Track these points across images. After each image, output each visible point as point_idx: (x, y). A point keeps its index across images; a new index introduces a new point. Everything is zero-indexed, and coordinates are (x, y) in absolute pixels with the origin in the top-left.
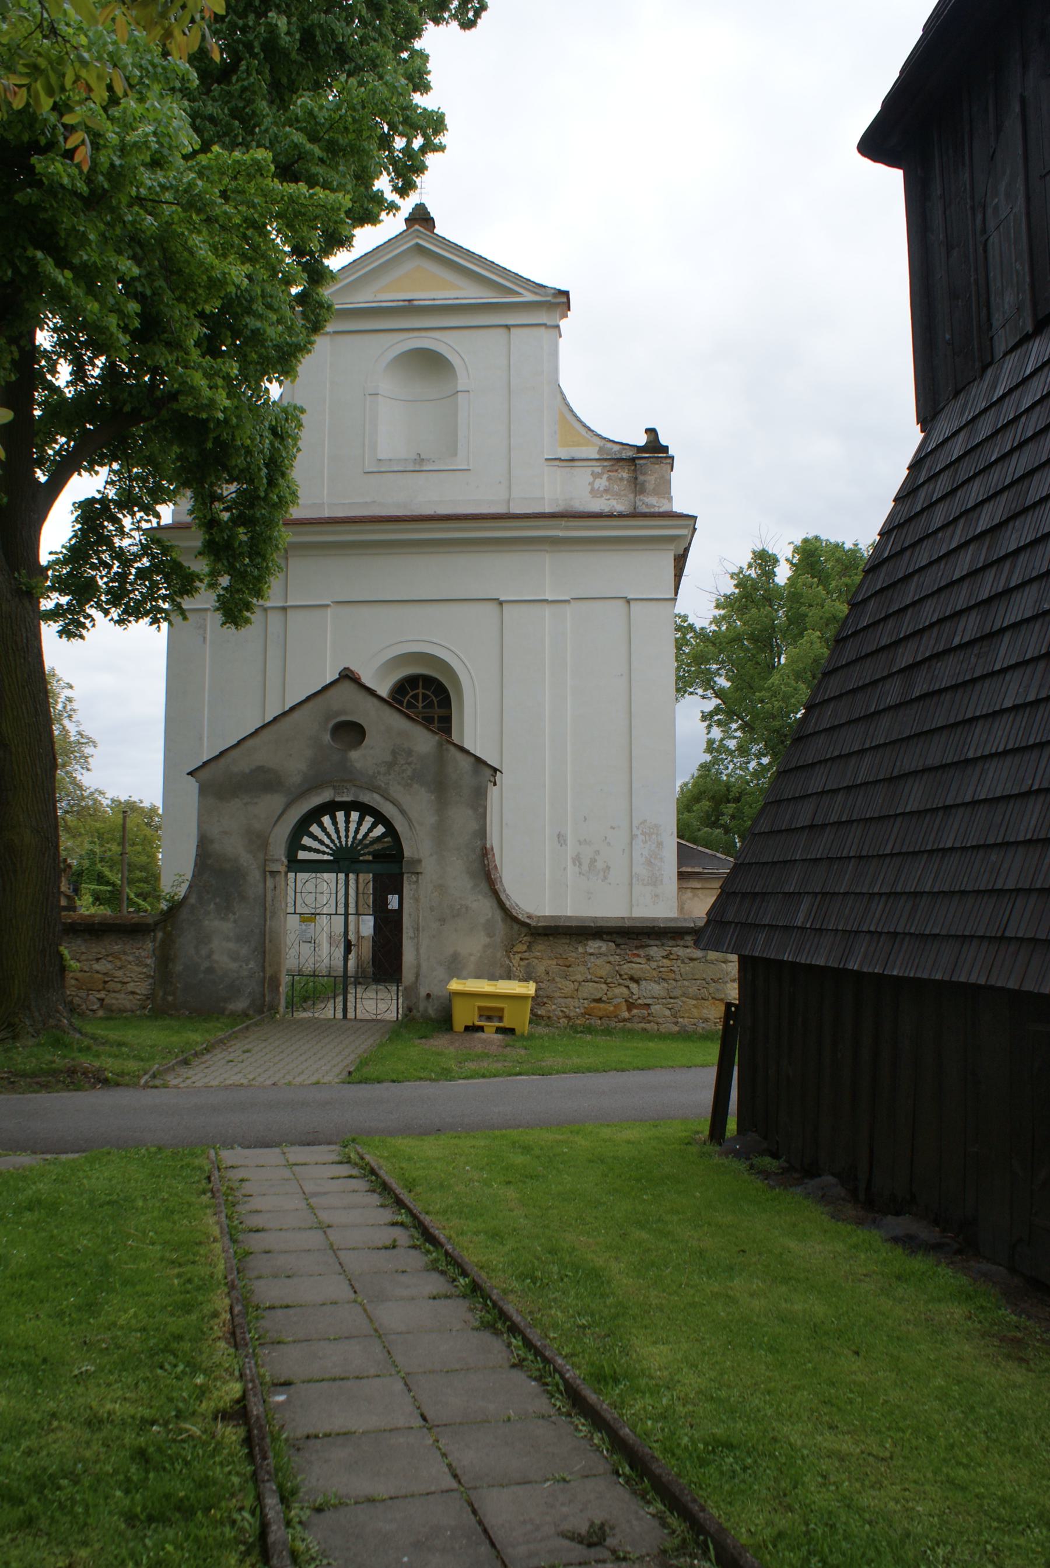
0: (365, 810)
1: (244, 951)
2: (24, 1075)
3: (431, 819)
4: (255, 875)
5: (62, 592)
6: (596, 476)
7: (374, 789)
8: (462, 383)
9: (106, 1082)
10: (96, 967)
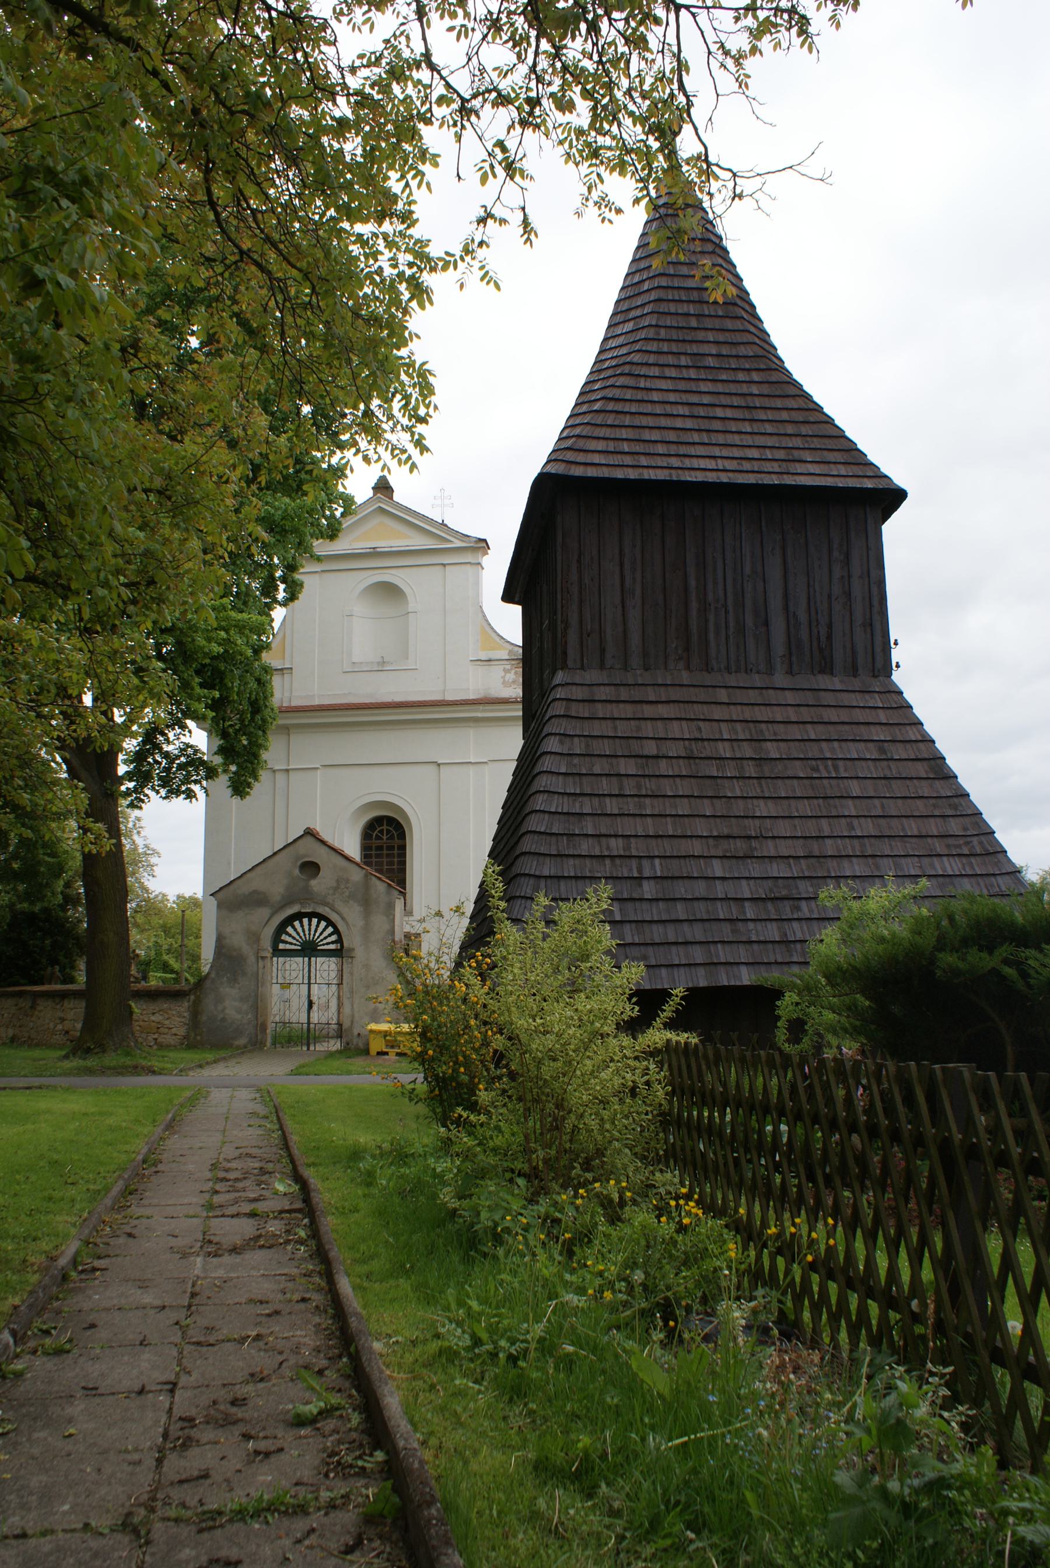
0: (321, 917)
1: (245, 1007)
2: (109, 1068)
3: (361, 923)
4: (252, 959)
5: (130, 780)
6: (506, 671)
7: (326, 904)
8: (412, 606)
9: (154, 1072)
10: (153, 1018)
